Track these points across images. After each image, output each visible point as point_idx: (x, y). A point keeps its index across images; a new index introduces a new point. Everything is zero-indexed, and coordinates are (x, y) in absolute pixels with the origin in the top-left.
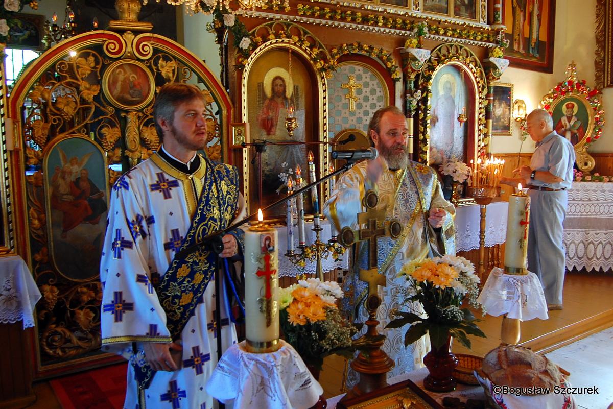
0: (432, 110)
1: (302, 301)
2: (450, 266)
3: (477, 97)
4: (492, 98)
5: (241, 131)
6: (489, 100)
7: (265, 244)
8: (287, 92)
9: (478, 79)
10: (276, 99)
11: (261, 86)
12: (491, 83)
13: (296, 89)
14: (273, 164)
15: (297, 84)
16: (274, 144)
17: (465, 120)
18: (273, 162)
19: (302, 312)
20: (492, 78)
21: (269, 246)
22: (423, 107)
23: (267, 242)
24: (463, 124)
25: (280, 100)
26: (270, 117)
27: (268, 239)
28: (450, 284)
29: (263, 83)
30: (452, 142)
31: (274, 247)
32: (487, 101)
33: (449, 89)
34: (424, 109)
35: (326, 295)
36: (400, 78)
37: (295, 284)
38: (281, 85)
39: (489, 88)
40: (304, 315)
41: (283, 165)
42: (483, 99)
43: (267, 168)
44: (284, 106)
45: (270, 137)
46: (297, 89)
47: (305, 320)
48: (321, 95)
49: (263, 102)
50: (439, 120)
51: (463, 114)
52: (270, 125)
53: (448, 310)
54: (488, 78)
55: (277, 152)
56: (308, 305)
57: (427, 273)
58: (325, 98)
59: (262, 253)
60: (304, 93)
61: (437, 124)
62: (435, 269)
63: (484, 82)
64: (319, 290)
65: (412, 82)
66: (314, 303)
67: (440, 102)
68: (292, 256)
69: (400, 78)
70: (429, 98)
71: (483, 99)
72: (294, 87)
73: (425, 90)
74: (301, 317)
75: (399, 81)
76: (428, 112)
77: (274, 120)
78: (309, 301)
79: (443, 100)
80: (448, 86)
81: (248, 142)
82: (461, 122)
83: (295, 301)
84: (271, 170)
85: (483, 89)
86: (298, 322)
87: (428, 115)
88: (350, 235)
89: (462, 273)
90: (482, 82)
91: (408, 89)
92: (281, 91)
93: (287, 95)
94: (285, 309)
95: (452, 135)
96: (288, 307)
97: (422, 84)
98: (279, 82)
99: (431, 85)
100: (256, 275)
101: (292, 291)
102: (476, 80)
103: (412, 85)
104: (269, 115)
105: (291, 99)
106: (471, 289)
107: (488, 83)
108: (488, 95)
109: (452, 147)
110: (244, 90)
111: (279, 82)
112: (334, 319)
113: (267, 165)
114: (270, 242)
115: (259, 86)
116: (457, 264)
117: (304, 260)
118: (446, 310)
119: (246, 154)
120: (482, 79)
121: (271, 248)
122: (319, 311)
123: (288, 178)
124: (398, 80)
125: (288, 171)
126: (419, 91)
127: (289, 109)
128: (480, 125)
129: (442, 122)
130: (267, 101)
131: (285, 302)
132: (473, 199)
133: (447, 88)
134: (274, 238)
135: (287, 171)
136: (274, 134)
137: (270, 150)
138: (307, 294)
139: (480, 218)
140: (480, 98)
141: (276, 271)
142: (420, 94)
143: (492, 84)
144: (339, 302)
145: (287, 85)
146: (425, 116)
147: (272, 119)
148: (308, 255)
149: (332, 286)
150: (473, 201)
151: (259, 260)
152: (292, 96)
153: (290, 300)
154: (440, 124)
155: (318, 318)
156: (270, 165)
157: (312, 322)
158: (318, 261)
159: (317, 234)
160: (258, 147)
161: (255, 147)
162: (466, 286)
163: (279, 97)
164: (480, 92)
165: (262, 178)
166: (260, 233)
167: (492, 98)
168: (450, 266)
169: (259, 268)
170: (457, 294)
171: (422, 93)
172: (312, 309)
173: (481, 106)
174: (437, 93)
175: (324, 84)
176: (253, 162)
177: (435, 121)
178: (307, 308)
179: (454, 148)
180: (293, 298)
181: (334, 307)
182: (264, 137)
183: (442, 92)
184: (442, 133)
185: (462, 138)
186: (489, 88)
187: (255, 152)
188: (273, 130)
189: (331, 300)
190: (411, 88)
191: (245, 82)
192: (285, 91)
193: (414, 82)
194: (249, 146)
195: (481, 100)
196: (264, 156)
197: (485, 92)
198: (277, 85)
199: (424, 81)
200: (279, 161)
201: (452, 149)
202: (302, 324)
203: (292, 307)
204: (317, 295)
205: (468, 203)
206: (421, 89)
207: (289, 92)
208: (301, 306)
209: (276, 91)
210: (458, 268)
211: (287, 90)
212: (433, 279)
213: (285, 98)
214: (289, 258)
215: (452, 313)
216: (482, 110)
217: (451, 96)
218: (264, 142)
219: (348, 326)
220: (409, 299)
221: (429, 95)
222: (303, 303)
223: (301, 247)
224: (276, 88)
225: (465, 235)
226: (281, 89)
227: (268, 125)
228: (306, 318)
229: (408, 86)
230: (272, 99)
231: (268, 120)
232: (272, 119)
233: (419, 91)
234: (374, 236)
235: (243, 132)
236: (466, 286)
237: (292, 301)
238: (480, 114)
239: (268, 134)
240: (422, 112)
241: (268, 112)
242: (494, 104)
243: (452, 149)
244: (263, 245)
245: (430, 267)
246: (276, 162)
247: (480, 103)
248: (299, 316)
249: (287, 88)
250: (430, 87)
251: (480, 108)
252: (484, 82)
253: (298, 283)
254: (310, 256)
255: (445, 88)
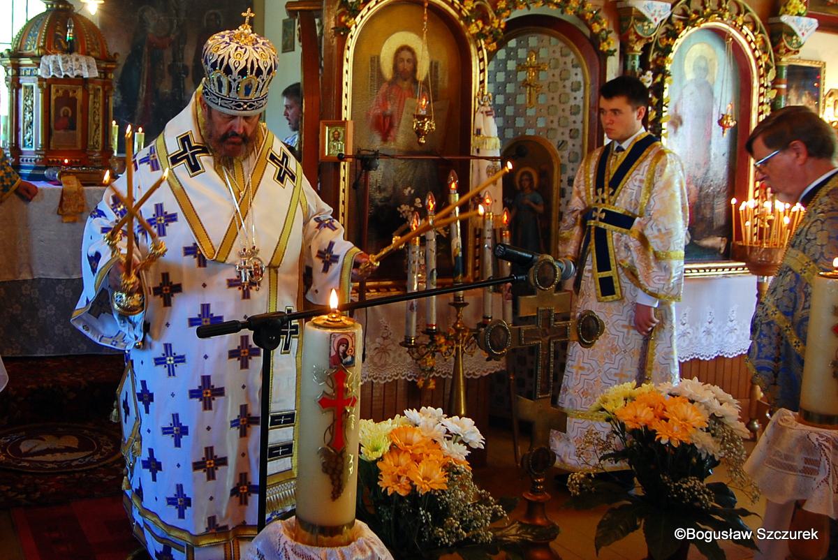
0: (671, 105)
1: (406, 451)
2: (692, 402)
3: (756, 84)
4: (784, 86)
5: (339, 134)
6: (779, 90)
7: (338, 352)
8: (418, 72)
9: (757, 54)
10: (400, 83)
11: (375, 61)
12: (784, 59)
13: (434, 67)
14: (390, 189)
15: (435, 59)
16: (393, 157)
17: (732, 124)
18: (390, 185)
19: (405, 472)
20: (784, 51)
21: (345, 356)
22: (655, 100)
23: (342, 348)
24: (727, 130)
25: (405, 85)
26: (388, 112)
27: (344, 342)
28: (690, 437)
29: (379, 57)
30: (707, 162)
31: (353, 357)
32: (775, 91)
33: (704, 69)
34: (658, 103)
35: (451, 442)
36: (615, 51)
37: (398, 416)
38: (408, 61)
39: (778, 68)
40: (408, 478)
41: (406, 192)
42: (767, 87)
43: (378, 196)
44: (413, 95)
45: (387, 145)
46: (436, 67)
47: (409, 487)
48: (476, 77)
49: (379, 88)
50: (684, 123)
51: (729, 113)
52: (387, 125)
53: (684, 486)
54: (776, 51)
55: (397, 171)
56: (417, 460)
57: (645, 415)
58: (482, 82)
59: (331, 367)
60: (447, 72)
61: (680, 129)
62: (661, 408)
63: (770, 58)
64: (439, 431)
65: (637, 58)
66: (428, 455)
67: (686, 92)
68: (412, 347)
69: (615, 51)
70: (666, 85)
71: (767, 87)
72: (431, 63)
73: (660, 70)
74: (403, 480)
75: (612, 55)
76: (664, 109)
77: (396, 117)
78: (419, 451)
79: (692, 88)
80: (703, 64)
81: (350, 153)
82: (724, 127)
83: (394, 448)
84: (387, 199)
85: (767, 69)
86: (397, 488)
87: (664, 114)
88: (502, 333)
89: (713, 416)
90: (765, 58)
91: (629, 68)
92: (408, 69)
93: (418, 77)
94: (376, 461)
95: (708, 150)
96: (381, 459)
97: (655, 61)
98: (406, 55)
99: (670, 62)
100: (318, 407)
101: (389, 431)
102: (754, 56)
103: (637, 63)
104: (387, 109)
105: (425, 83)
106: (730, 451)
107: (777, 60)
108: (776, 82)
109: (708, 170)
110: (348, 67)
111: (406, 55)
112: (463, 486)
113: (380, 189)
114: (347, 347)
115: (372, 60)
116: (706, 400)
117: (434, 356)
118: (680, 487)
119: (344, 172)
120: (765, 53)
121: (349, 359)
122: (434, 472)
123: (413, 213)
124: (611, 53)
125: (414, 202)
126: (649, 73)
127: (420, 99)
128: (762, 104)
129: (690, 126)
130: (384, 87)
131: (376, 450)
132: (744, 264)
133: (700, 68)
134: (354, 341)
135: (412, 203)
136: (395, 140)
137: (386, 167)
138: (416, 438)
139: (756, 299)
140: (762, 85)
141: (355, 400)
142: (651, 78)
143: (785, 61)
144: (475, 457)
145: (419, 59)
146: (659, 115)
147: (391, 116)
148: (441, 346)
149: (463, 427)
150: (744, 268)
151: (322, 377)
152: (427, 78)
153: (385, 447)
154: (686, 129)
155: (432, 486)
156: (384, 190)
157: (422, 493)
158: (456, 358)
159: (458, 311)
160: (364, 162)
161: (359, 161)
162: (722, 443)
163: (405, 80)
164: (761, 76)
165: (369, 211)
166: (330, 331)
167: (784, 86)
168: (692, 402)
169: (324, 392)
170: (704, 456)
171: (654, 77)
172: (422, 468)
173: (762, 100)
174: (682, 77)
175: (482, 60)
176: (358, 185)
177: (677, 122)
178: (413, 466)
179: (711, 174)
180: (390, 443)
181: (464, 467)
182: (377, 143)
183: (690, 75)
184: (689, 146)
185: (726, 155)
186: (778, 68)
187: (359, 168)
188: (392, 133)
189: (459, 453)
190: (633, 67)
191: (349, 54)
192: (414, 70)
193: (641, 57)
194: (351, 160)
195: (762, 90)
196: (376, 176)
197: (771, 75)
198: (403, 60)
199: (658, 56)
200: (400, 186)
201: (706, 174)
202: (403, 493)
203: (387, 460)
204: (435, 442)
205: (733, 271)
206: (652, 70)
207: (423, 71)
208: (404, 460)
209: (401, 69)
210: (707, 408)
211: (418, 69)
212: (658, 426)
213: (415, 82)
214: (407, 349)
215: (692, 494)
216: (765, 107)
217: (707, 82)
218: (376, 155)
219: (487, 503)
220: (610, 455)
221: (667, 79)
222: (407, 456)
223: (428, 332)
224: (401, 65)
225: (727, 328)
226: (408, 66)
227: (384, 126)
228: (411, 482)
229: (630, 64)
230: (393, 83)
231: (385, 116)
232: (391, 116)
233: (649, 73)
234: (548, 338)
235: (342, 135)
236: (722, 443)
237: (387, 449)
238: (760, 113)
239: (385, 139)
240: (654, 109)
241: (384, 105)
242: (787, 95)
243: (706, 174)
244: (333, 353)
245: (653, 402)
246: (394, 188)
247: (761, 95)
248: (399, 477)
249: (419, 64)
250: (668, 67)
251: (762, 104)
252: (770, 58)
253: (404, 415)
254: (444, 349)
255: (696, 68)
